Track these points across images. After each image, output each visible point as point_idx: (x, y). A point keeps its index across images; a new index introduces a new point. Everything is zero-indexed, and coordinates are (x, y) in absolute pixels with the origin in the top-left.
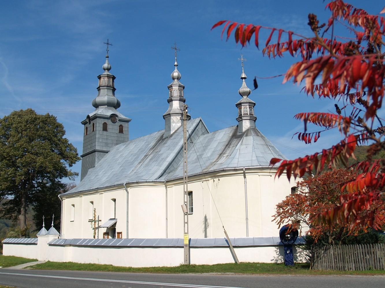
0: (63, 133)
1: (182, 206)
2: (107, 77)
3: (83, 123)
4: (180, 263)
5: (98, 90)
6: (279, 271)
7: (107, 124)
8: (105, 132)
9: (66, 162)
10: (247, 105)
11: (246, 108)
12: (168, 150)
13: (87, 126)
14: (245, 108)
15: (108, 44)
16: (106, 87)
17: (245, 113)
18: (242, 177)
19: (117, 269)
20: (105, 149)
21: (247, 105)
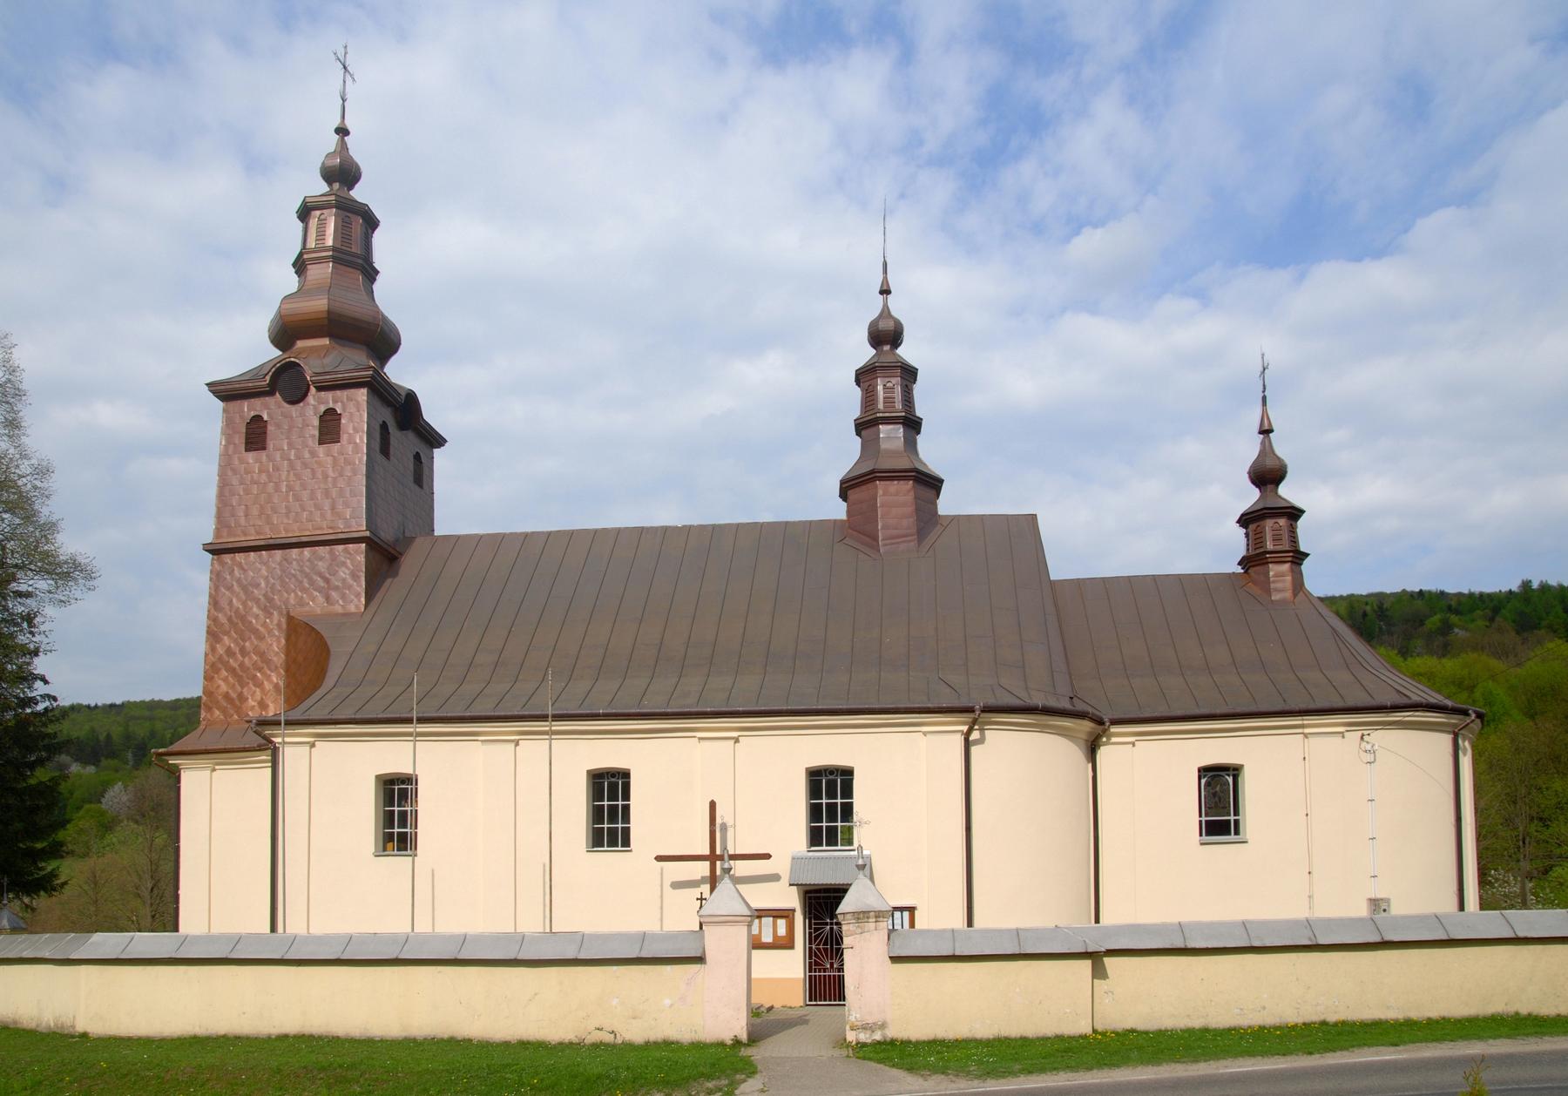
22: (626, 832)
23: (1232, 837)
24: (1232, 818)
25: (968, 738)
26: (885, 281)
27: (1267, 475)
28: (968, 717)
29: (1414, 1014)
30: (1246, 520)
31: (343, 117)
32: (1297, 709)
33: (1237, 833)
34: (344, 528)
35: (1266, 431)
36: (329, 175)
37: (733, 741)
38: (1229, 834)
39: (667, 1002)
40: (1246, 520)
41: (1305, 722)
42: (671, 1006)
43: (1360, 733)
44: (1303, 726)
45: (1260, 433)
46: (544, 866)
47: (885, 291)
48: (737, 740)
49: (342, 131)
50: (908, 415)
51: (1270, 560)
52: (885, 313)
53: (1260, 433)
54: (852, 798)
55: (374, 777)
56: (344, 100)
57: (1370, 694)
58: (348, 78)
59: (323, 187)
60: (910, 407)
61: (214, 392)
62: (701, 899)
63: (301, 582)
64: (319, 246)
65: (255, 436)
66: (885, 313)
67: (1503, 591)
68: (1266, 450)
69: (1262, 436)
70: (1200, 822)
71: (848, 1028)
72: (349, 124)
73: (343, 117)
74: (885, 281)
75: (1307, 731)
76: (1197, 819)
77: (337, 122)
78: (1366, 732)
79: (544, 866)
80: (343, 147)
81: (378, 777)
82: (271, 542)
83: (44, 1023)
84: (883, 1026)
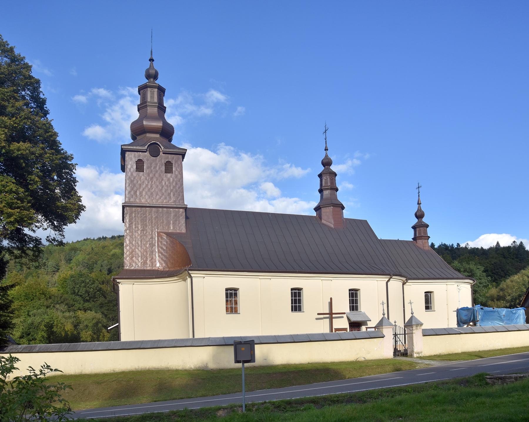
22: (300, 307)
23: (430, 310)
24: (430, 305)
25: (388, 283)
26: (326, 147)
27: (419, 215)
28: (389, 277)
30: (414, 228)
31: (152, 54)
33: (431, 309)
34: (156, 202)
35: (419, 204)
36: (148, 76)
38: (429, 309)
39: (376, 349)
40: (414, 228)
42: (377, 350)
43: (457, 285)
45: (418, 204)
47: (326, 150)
48: (270, 279)
49: (151, 60)
50: (331, 187)
51: (423, 238)
53: (418, 204)
57: (277, 267)
62: (395, 322)
63: (135, 217)
64: (151, 101)
66: (326, 156)
68: (419, 210)
70: (431, 304)
71: (414, 353)
73: (152, 54)
74: (326, 147)
75: (447, 283)
78: (459, 284)
82: (151, 205)
83: (148, 368)
84: (421, 353)
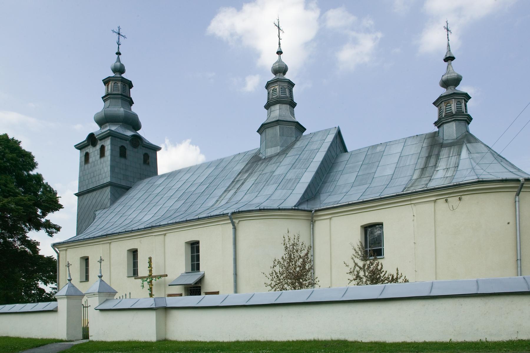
0: (33, 166)
1: (80, 282)
2: (121, 81)
3: (79, 147)
4: (47, 337)
5: (104, 101)
6: (6, 347)
7: (126, 149)
8: (123, 160)
9: (451, 90)
10: (462, 99)
11: (460, 103)
12: (294, 169)
13: (88, 151)
14: (458, 103)
15: (119, 34)
16: (120, 96)
17: (447, 112)
18: (433, 203)
19: (51, 341)
20: (123, 183)
21: (462, 99)
29: (491, 339)
32: (500, 178)
36: (115, 70)
37: (329, 220)
41: (412, 198)
44: (411, 200)
46: (85, 302)
52: (280, 60)
54: (199, 262)
55: (359, 228)
56: (119, 45)
58: (449, 33)
59: (112, 74)
60: (290, 93)
61: (76, 148)
65: (87, 158)
66: (280, 60)
67: (21, 145)
69: (446, 63)
72: (283, 49)
76: (384, 247)
77: (276, 49)
79: (85, 302)
80: (119, 60)
81: (361, 226)
